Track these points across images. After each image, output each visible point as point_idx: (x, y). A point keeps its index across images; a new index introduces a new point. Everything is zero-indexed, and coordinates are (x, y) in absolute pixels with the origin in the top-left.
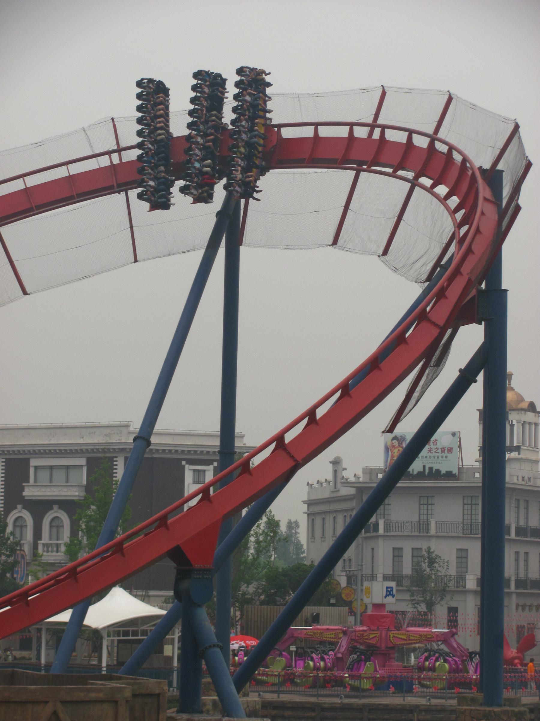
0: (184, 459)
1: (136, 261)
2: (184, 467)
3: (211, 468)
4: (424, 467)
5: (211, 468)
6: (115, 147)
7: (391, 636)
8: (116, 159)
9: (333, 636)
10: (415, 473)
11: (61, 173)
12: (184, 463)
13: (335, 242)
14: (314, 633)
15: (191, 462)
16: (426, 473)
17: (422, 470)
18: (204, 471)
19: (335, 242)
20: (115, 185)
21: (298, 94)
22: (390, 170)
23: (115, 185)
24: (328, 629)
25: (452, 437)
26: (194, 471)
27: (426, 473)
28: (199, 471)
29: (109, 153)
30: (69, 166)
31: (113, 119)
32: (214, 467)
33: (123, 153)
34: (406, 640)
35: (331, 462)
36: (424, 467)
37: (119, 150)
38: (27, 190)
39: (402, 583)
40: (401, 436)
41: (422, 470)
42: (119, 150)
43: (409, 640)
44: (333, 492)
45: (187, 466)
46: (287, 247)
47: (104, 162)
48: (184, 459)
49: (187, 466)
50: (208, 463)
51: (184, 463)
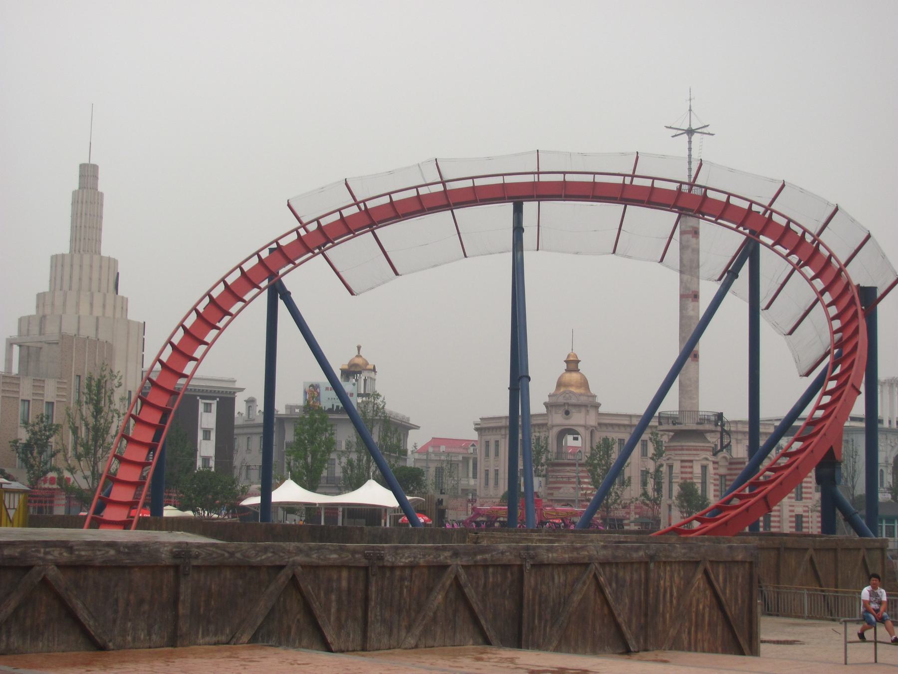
0: (198, 396)
1: (538, 250)
2: (198, 401)
3: (215, 402)
4: (333, 405)
5: (215, 402)
6: (536, 171)
7: (545, 513)
8: (628, 181)
9: (505, 513)
10: (326, 409)
11: (499, 180)
12: (198, 398)
13: (614, 252)
14: (493, 511)
15: (203, 398)
16: (334, 409)
17: (331, 407)
18: (211, 404)
19: (614, 252)
20: (563, 195)
21: (570, 153)
22: (714, 219)
23: (563, 195)
24: (501, 509)
25: (130, 390)
26: (205, 403)
27: (334, 409)
28: (207, 404)
29: (625, 175)
30: (505, 177)
31: (538, 151)
32: (217, 401)
33: (540, 175)
34: (555, 516)
35: (245, 401)
36: (333, 405)
37: (538, 173)
38: (474, 188)
39: (442, 480)
40: (316, 385)
41: (331, 407)
42: (538, 173)
43: (558, 516)
44: (246, 421)
45: (200, 400)
46: (577, 253)
47: (619, 180)
48: (198, 396)
49: (200, 400)
50: (213, 398)
51: (198, 398)
